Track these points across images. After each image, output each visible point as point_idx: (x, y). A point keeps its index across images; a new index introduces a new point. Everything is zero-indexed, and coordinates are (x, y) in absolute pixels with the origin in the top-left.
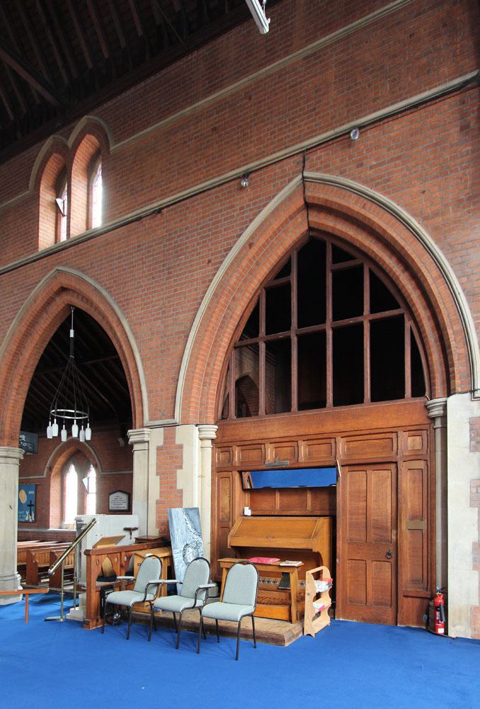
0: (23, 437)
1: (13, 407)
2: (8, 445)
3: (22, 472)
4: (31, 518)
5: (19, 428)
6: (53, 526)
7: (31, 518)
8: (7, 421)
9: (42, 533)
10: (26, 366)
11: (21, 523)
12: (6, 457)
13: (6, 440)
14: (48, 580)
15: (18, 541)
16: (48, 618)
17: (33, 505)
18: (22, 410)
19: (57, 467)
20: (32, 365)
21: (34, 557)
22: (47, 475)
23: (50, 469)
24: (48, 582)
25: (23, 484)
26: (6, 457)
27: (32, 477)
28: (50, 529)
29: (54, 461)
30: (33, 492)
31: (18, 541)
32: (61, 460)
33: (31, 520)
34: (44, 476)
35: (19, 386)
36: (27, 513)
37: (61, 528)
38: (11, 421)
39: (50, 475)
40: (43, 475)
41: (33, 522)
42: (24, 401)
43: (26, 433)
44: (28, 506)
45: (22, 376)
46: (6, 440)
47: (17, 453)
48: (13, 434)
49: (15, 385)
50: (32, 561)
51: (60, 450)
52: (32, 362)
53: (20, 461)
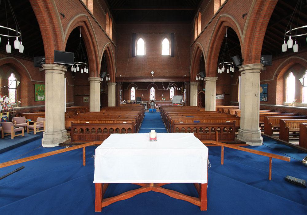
0: (263, 58)
1: (257, 42)
2: (254, 63)
3: (262, 78)
4: (266, 100)
5: (260, 53)
6: (279, 104)
7: (266, 100)
8: (253, 51)
9: (272, 107)
10: (265, 16)
11: (261, 102)
12: (253, 69)
13: (253, 60)
14: (278, 133)
15: (260, 110)
16: (289, 177)
17: (266, 94)
18: (262, 43)
19: (281, 74)
20: (269, 14)
21: (269, 121)
22: (274, 78)
23: (277, 76)
24: (278, 135)
25: (262, 84)
26: (253, 69)
27: (265, 81)
28: (277, 105)
29: (279, 72)
30: (266, 88)
31: (260, 110)
32: (283, 71)
33: (265, 100)
34: (236, 84)
35: (260, 29)
36: (263, 97)
37: (283, 105)
38: (256, 50)
39: (277, 79)
40: (272, 79)
41: (266, 101)
42: (263, 37)
43: (264, 56)
44: (264, 94)
45: (262, 23)
46: (253, 60)
47: (259, 66)
48: (257, 57)
49: (258, 29)
50: (268, 123)
51: (283, 65)
52: (268, 12)
53: (261, 71)
